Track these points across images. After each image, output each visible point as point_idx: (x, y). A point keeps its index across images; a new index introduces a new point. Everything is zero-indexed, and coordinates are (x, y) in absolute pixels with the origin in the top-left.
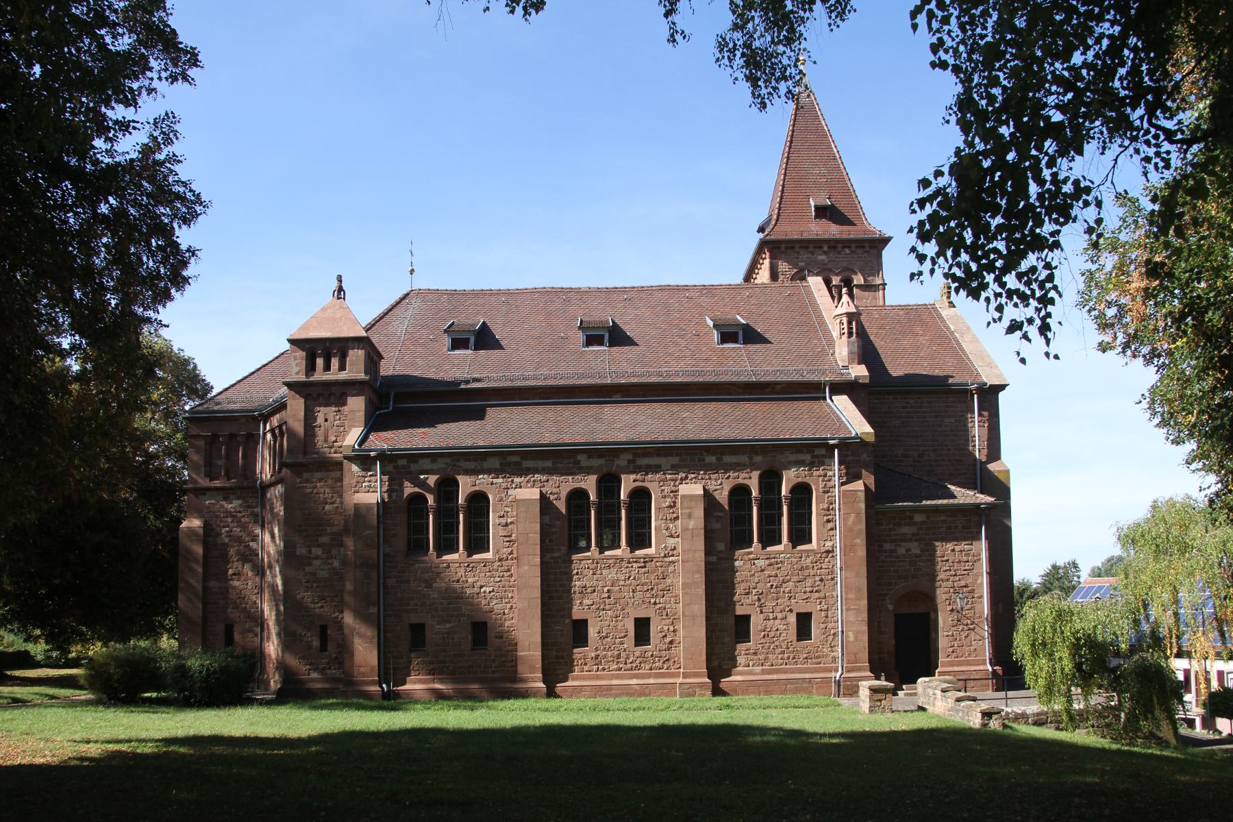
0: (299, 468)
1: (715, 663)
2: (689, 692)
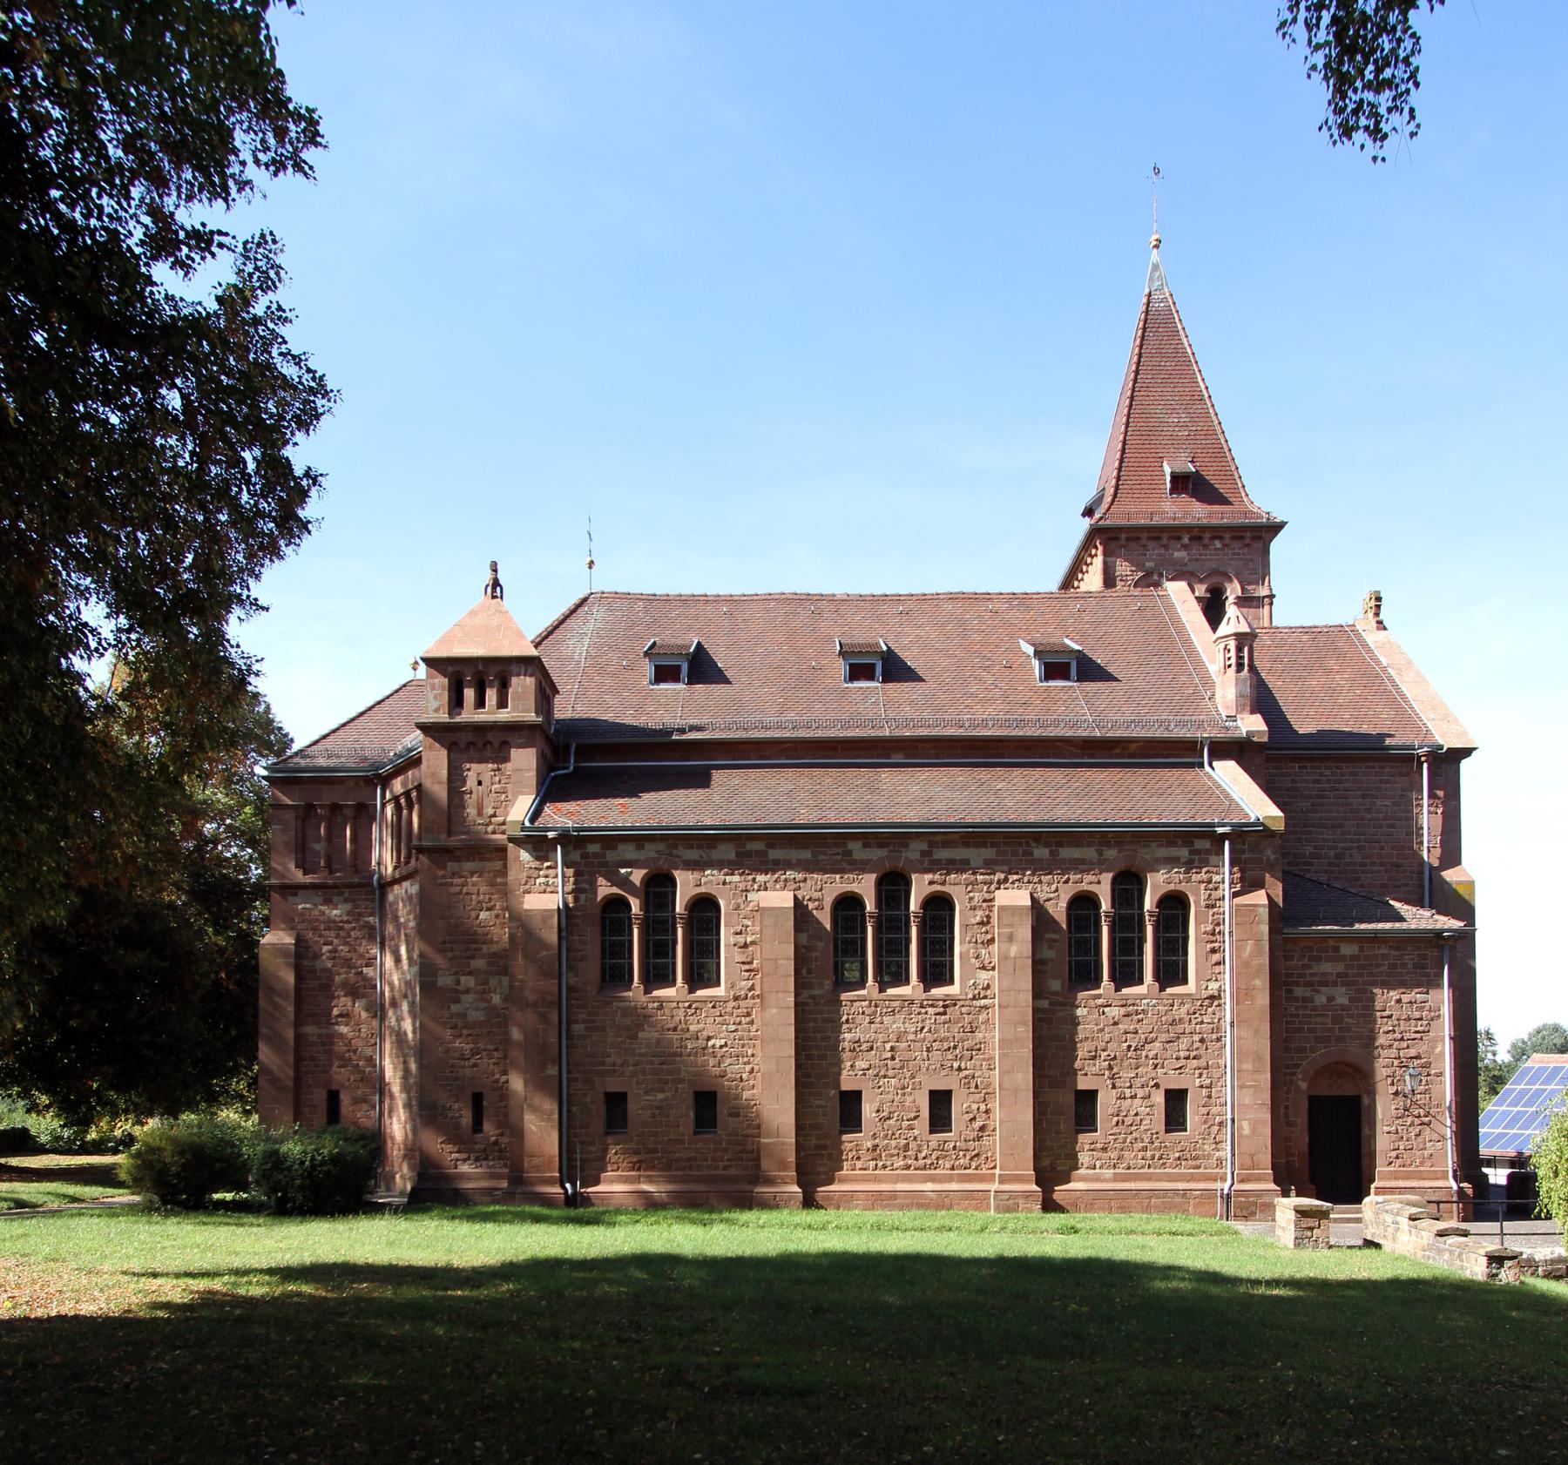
0: (442, 854)
1: (1046, 1162)
2: (1008, 1205)
